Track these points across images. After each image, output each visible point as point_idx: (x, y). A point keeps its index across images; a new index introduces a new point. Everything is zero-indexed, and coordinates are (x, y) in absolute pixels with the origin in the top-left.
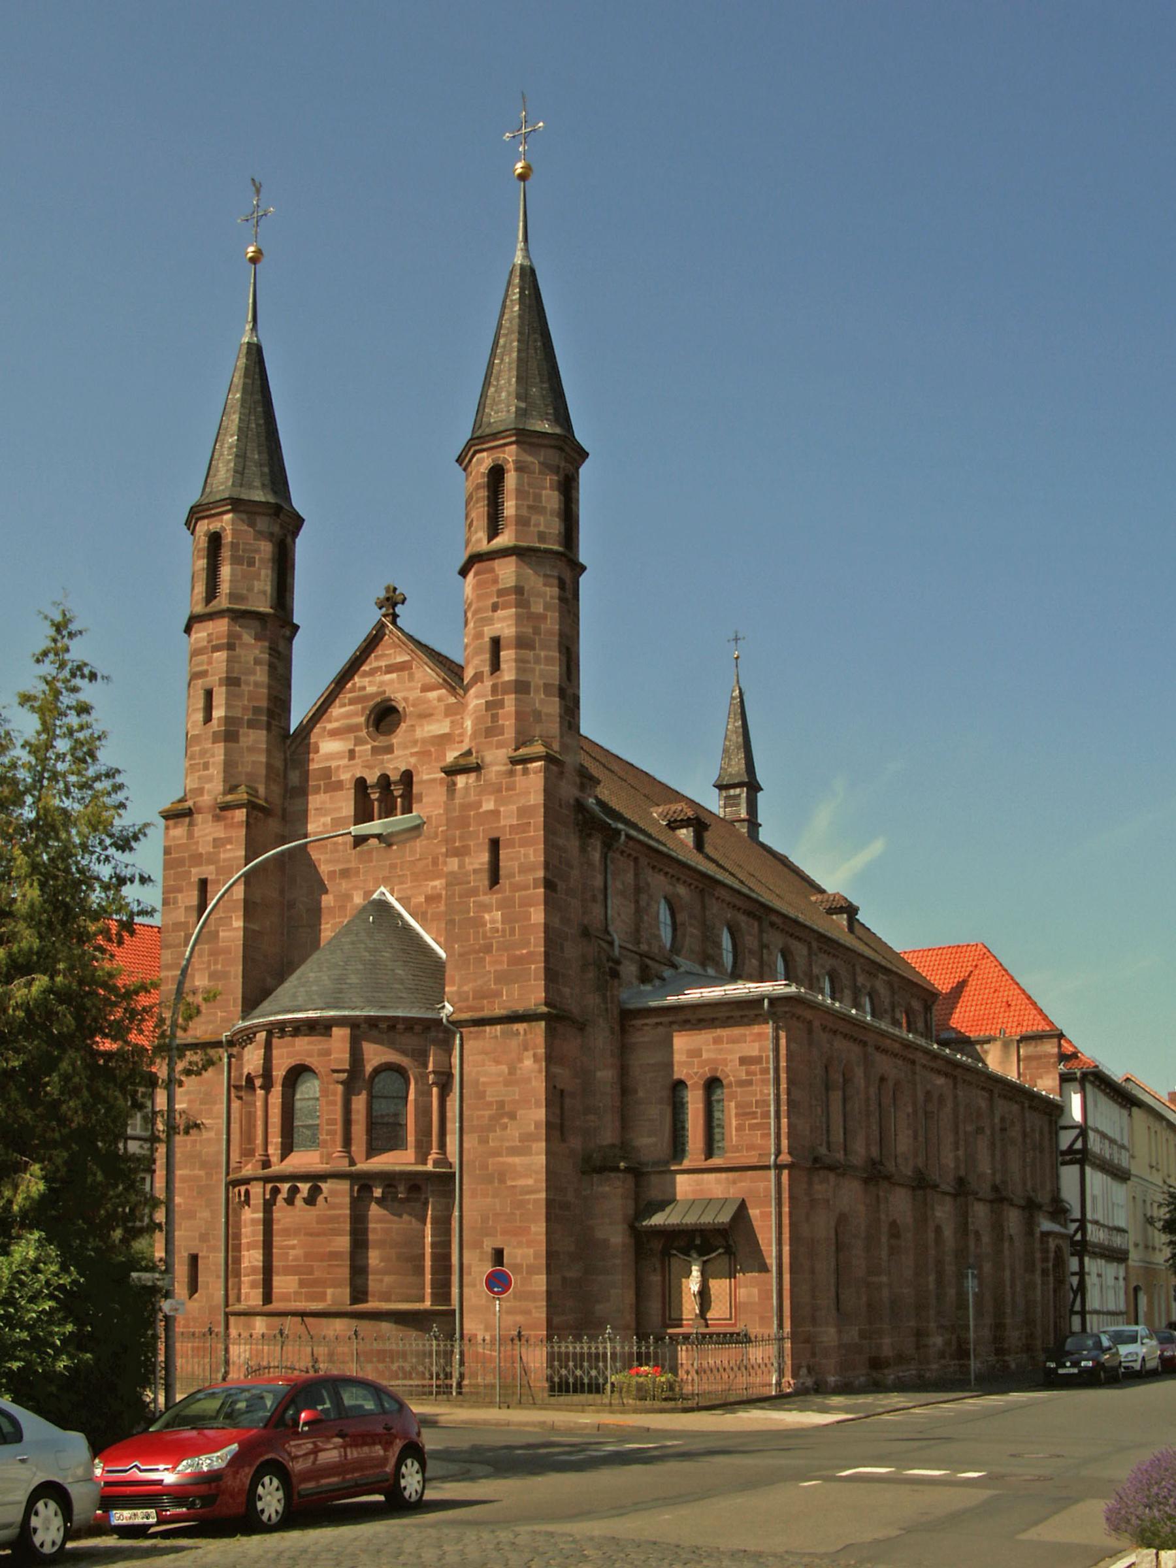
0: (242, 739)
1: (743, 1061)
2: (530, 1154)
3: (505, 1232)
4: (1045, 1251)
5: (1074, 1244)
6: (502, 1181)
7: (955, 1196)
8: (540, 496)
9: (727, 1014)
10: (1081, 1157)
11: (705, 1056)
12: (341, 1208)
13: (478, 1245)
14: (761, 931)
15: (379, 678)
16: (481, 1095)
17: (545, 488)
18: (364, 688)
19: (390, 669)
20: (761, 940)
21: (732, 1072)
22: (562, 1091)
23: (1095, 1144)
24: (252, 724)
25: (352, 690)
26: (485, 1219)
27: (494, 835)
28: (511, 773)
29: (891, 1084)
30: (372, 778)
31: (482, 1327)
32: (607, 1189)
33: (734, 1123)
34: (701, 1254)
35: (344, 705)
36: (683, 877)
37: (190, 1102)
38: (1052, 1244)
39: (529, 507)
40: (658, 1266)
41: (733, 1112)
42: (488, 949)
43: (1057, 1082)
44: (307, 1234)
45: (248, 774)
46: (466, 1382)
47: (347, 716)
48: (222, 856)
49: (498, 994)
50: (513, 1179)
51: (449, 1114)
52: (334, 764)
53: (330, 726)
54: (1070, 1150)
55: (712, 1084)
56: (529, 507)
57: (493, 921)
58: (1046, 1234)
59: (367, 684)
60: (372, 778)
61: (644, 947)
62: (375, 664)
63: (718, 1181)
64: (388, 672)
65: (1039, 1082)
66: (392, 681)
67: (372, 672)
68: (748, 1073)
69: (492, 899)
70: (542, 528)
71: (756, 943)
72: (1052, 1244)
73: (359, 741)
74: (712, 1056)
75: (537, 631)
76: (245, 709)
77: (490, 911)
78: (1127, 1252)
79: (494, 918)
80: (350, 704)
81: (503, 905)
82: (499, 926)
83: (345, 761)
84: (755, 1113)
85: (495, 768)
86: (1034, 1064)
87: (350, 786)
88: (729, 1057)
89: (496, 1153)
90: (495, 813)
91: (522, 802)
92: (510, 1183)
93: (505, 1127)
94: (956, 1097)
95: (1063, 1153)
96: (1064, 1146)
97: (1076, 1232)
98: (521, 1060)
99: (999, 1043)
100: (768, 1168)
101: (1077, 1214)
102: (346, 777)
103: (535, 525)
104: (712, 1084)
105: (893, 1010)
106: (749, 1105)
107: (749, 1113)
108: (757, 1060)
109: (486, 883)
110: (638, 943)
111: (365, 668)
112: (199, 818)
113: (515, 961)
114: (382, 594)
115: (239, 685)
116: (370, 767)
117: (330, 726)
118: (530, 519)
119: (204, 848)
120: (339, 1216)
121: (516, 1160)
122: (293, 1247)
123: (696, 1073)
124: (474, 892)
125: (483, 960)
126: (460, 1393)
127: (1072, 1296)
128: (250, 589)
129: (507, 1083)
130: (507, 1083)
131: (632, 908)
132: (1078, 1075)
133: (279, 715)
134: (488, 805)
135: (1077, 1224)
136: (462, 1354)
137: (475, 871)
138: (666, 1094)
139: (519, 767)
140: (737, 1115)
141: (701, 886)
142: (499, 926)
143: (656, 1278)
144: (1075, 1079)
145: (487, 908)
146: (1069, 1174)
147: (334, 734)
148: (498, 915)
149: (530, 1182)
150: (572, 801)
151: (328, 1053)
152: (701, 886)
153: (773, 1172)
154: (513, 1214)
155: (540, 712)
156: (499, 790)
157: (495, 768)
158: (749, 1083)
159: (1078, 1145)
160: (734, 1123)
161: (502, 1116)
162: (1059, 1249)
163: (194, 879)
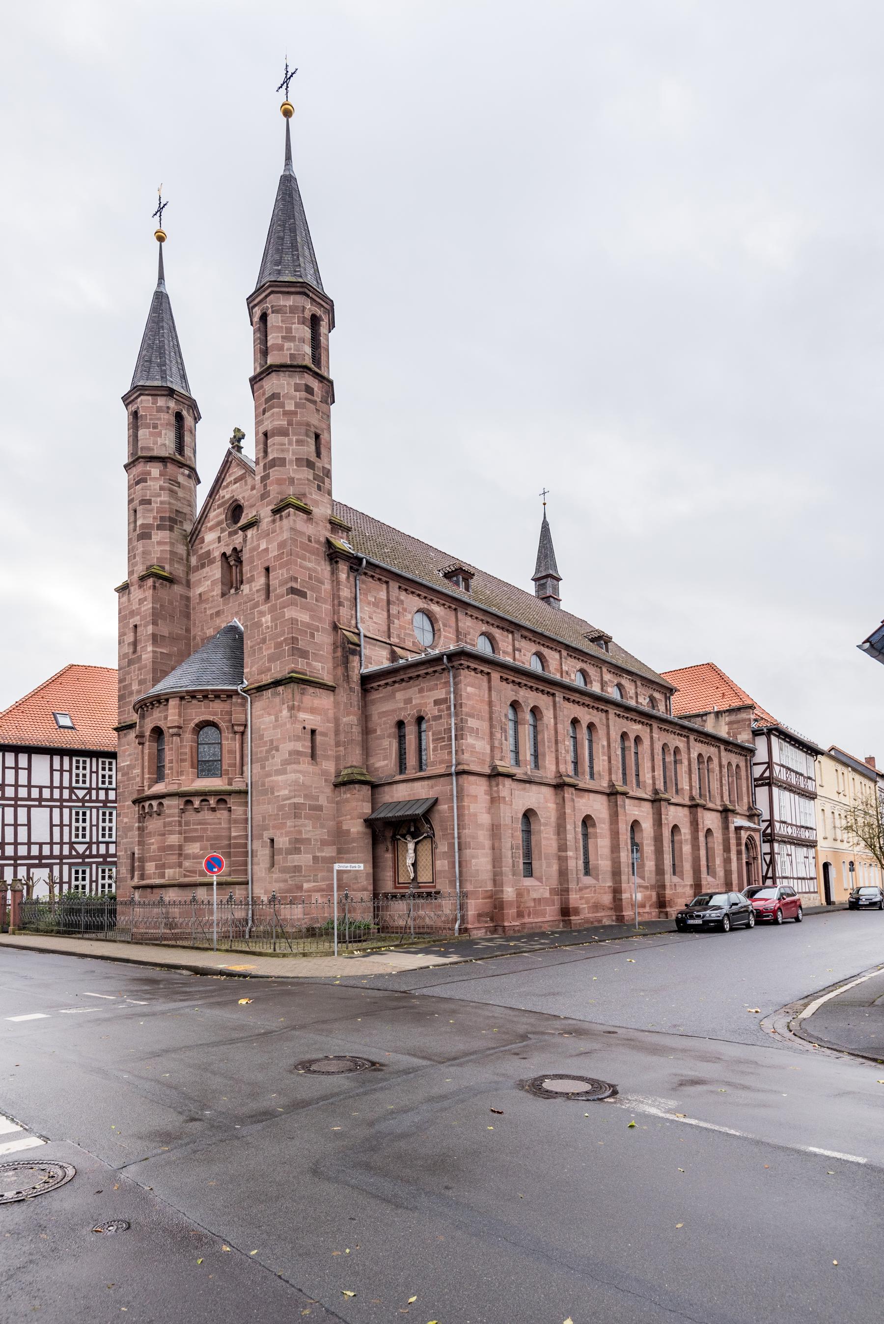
0: (153, 537)
1: (437, 702)
2: (286, 773)
3: (274, 827)
4: (739, 839)
5: (765, 834)
6: (273, 793)
7: (653, 801)
8: (291, 328)
9: (425, 671)
10: (768, 782)
11: (414, 703)
12: (173, 817)
13: (261, 837)
14: (513, 640)
15: (230, 489)
16: (261, 737)
17: (294, 323)
18: (224, 497)
19: (236, 481)
20: (514, 646)
21: (431, 711)
22: (313, 732)
23: (780, 773)
24: (159, 527)
25: (219, 500)
26: (264, 819)
27: (266, 565)
28: (274, 521)
29: (584, 725)
30: (229, 552)
31: (263, 891)
32: (349, 795)
33: (431, 746)
34: (413, 838)
35: (215, 510)
36: (496, 624)
37: (131, 760)
38: (744, 835)
39: (283, 337)
40: (390, 847)
41: (431, 738)
42: (264, 641)
43: (751, 736)
44: (159, 835)
45: (158, 558)
46: (254, 929)
47: (217, 516)
48: (143, 609)
49: (269, 670)
50: (278, 791)
51: (245, 752)
52: (211, 548)
53: (209, 525)
54: (761, 778)
55: (420, 720)
56: (283, 337)
57: (266, 622)
58: (738, 829)
59: (225, 494)
60: (229, 552)
61: (394, 640)
62: (229, 480)
63: (423, 788)
64: (235, 483)
65: (739, 737)
66: (237, 488)
67: (227, 486)
68: (439, 711)
69: (264, 608)
70: (292, 352)
71: (511, 647)
72: (744, 835)
73: (223, 530)
74: (418, 701)
75: (290, 423)
76: (154, 518)
77: (265, 616)
78: (816, 842)
79: (267, 620)
80: (218, 508)
81: (272, 610)
82: (269, 624)
83: (216, 545)
84: (444, 738)
85: (266, 520)
86: (735, 726)
87: (218, 558)
88: (428, 701)
89: (269, 775)
90: (267, 550)
91: (280, 539)
92: (276, 794)
93: (273, 757)
94: (652, 738)
95: (756, 780)
96: (757, 775)
97: (767, 828)
98: (281, 711)
99: (712, 715)
100: (450, 775)
101: (766, 816)
102: (217, 554)
103: (287, 350)
104: (420, 720)
105: (637, 697)
106: (440, 733)
107: (440, 739)
108: (445, 701)
109: (263, 597)
110: (389, 637)
111: (224, 484)
112: (132, 589)
113: (278, 645)
114: (232, 435)
115: (150, 504)
116: (227, 545)
117: (209, 525)
118: (283, 346)
119: (135, 606)
120: (173, 821)
121: (280, 778)
122: (153, 844)
123: (409, 715)
124: (256, 605)
125: (261, 649)
126: (250, 937)
127: (765, 867)
128: (155, 443)
129: (275, 728)
130: (275, 728)
131: (385, 614)
132: (765, 730)
133: (181, 522)
134: (263, 546)
135: (767, 823)
136: (253, 911)
137: (258, 591)
138: (394, 730)
139: (278, 516)
140: (433, 740)
141: (454, 606)
142: (269, 624)
143: (389, 856)
144: (763, 734)
145: (262, 614)
146: (762, 793)
147: (211, 529)
148: (269, 617)
149: (286, 792)
150: (323, 539)
151: (166, 718)
152: (454, 606)
153: (454, 778)
154: (278, 814)
155: (293, 478)
156: (268, 535)
157: (266, 520)
158: (440, 717)
159: (767, 774)
160: (431, 746)
161: (271, 749)
162: (750, 838)
163: (131, 626)
